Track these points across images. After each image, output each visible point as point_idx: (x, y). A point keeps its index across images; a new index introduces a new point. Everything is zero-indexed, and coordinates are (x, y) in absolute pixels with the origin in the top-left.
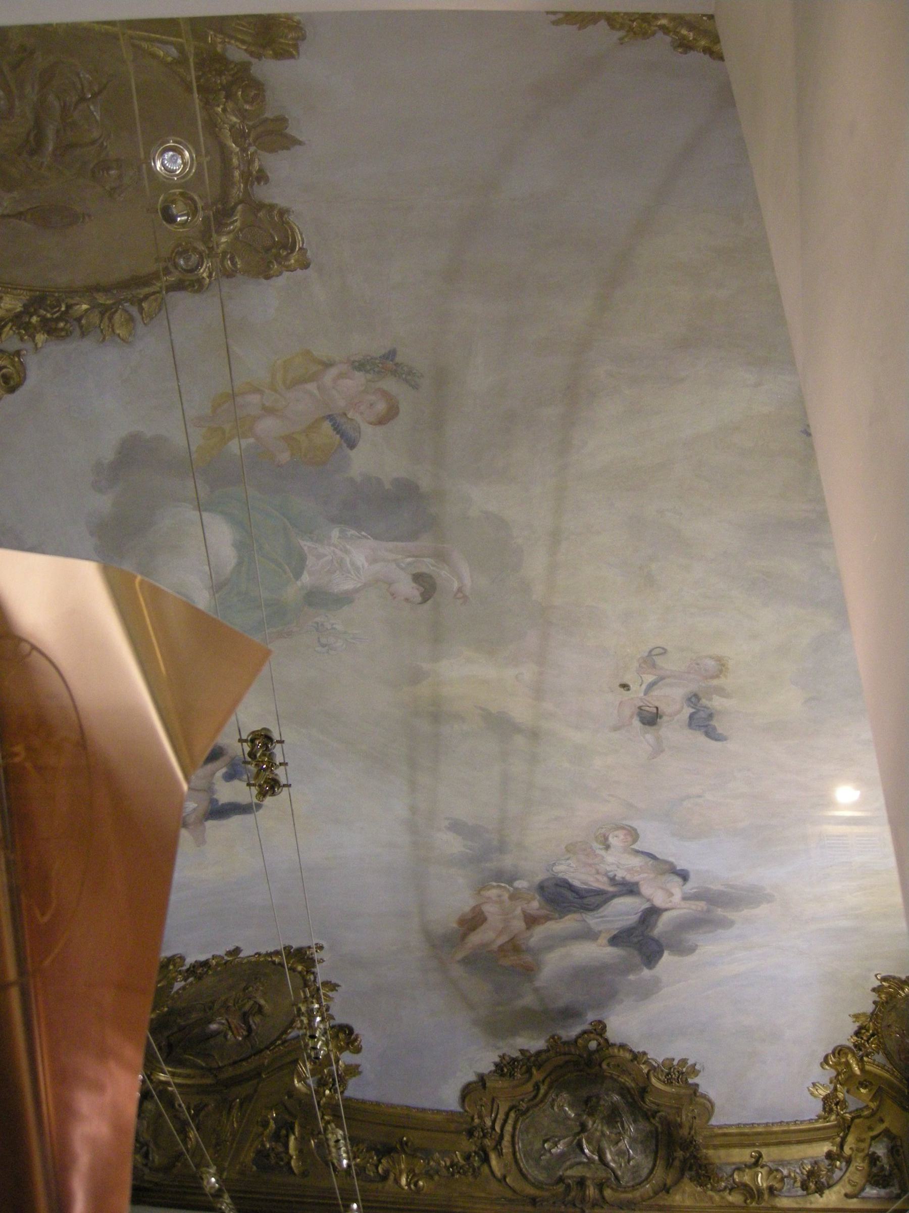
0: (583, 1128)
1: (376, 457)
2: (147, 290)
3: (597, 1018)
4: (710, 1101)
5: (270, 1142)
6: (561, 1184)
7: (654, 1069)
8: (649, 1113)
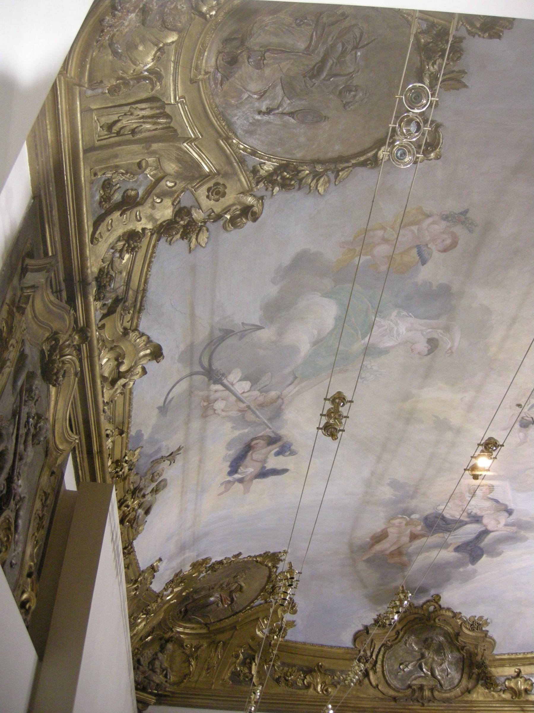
0: (423, 656)
1: (434, 272)
3: (436, 593)
4: (494, 640)
5: (240, 667)
8: (460, 648)
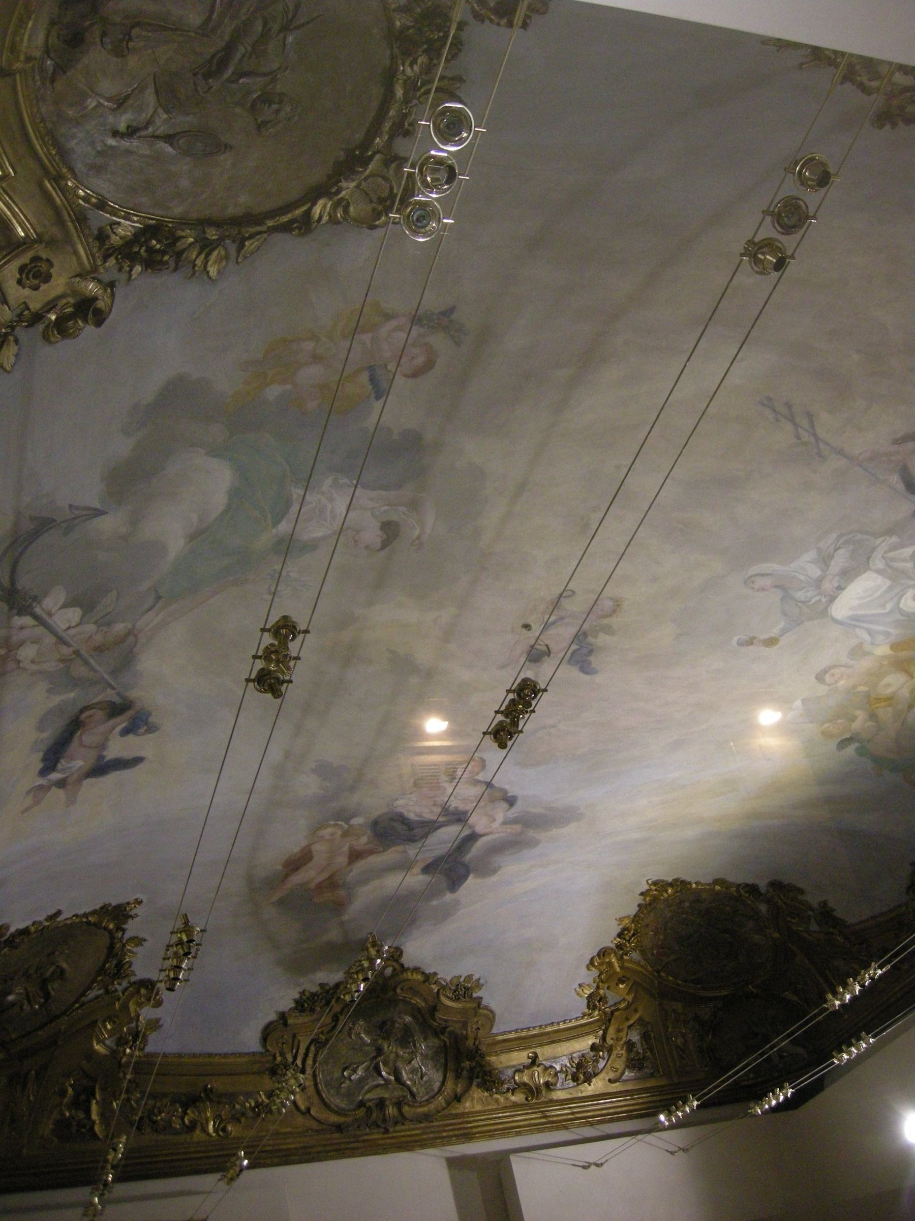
0: (379, 1051)
1: (401, 410)
2: (252, 230)
4: (492, 1011)
5: (70, 1111)
6: (362, 1109)
7: (444, 987)
